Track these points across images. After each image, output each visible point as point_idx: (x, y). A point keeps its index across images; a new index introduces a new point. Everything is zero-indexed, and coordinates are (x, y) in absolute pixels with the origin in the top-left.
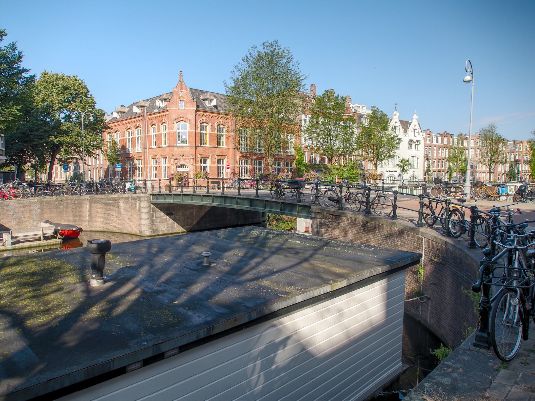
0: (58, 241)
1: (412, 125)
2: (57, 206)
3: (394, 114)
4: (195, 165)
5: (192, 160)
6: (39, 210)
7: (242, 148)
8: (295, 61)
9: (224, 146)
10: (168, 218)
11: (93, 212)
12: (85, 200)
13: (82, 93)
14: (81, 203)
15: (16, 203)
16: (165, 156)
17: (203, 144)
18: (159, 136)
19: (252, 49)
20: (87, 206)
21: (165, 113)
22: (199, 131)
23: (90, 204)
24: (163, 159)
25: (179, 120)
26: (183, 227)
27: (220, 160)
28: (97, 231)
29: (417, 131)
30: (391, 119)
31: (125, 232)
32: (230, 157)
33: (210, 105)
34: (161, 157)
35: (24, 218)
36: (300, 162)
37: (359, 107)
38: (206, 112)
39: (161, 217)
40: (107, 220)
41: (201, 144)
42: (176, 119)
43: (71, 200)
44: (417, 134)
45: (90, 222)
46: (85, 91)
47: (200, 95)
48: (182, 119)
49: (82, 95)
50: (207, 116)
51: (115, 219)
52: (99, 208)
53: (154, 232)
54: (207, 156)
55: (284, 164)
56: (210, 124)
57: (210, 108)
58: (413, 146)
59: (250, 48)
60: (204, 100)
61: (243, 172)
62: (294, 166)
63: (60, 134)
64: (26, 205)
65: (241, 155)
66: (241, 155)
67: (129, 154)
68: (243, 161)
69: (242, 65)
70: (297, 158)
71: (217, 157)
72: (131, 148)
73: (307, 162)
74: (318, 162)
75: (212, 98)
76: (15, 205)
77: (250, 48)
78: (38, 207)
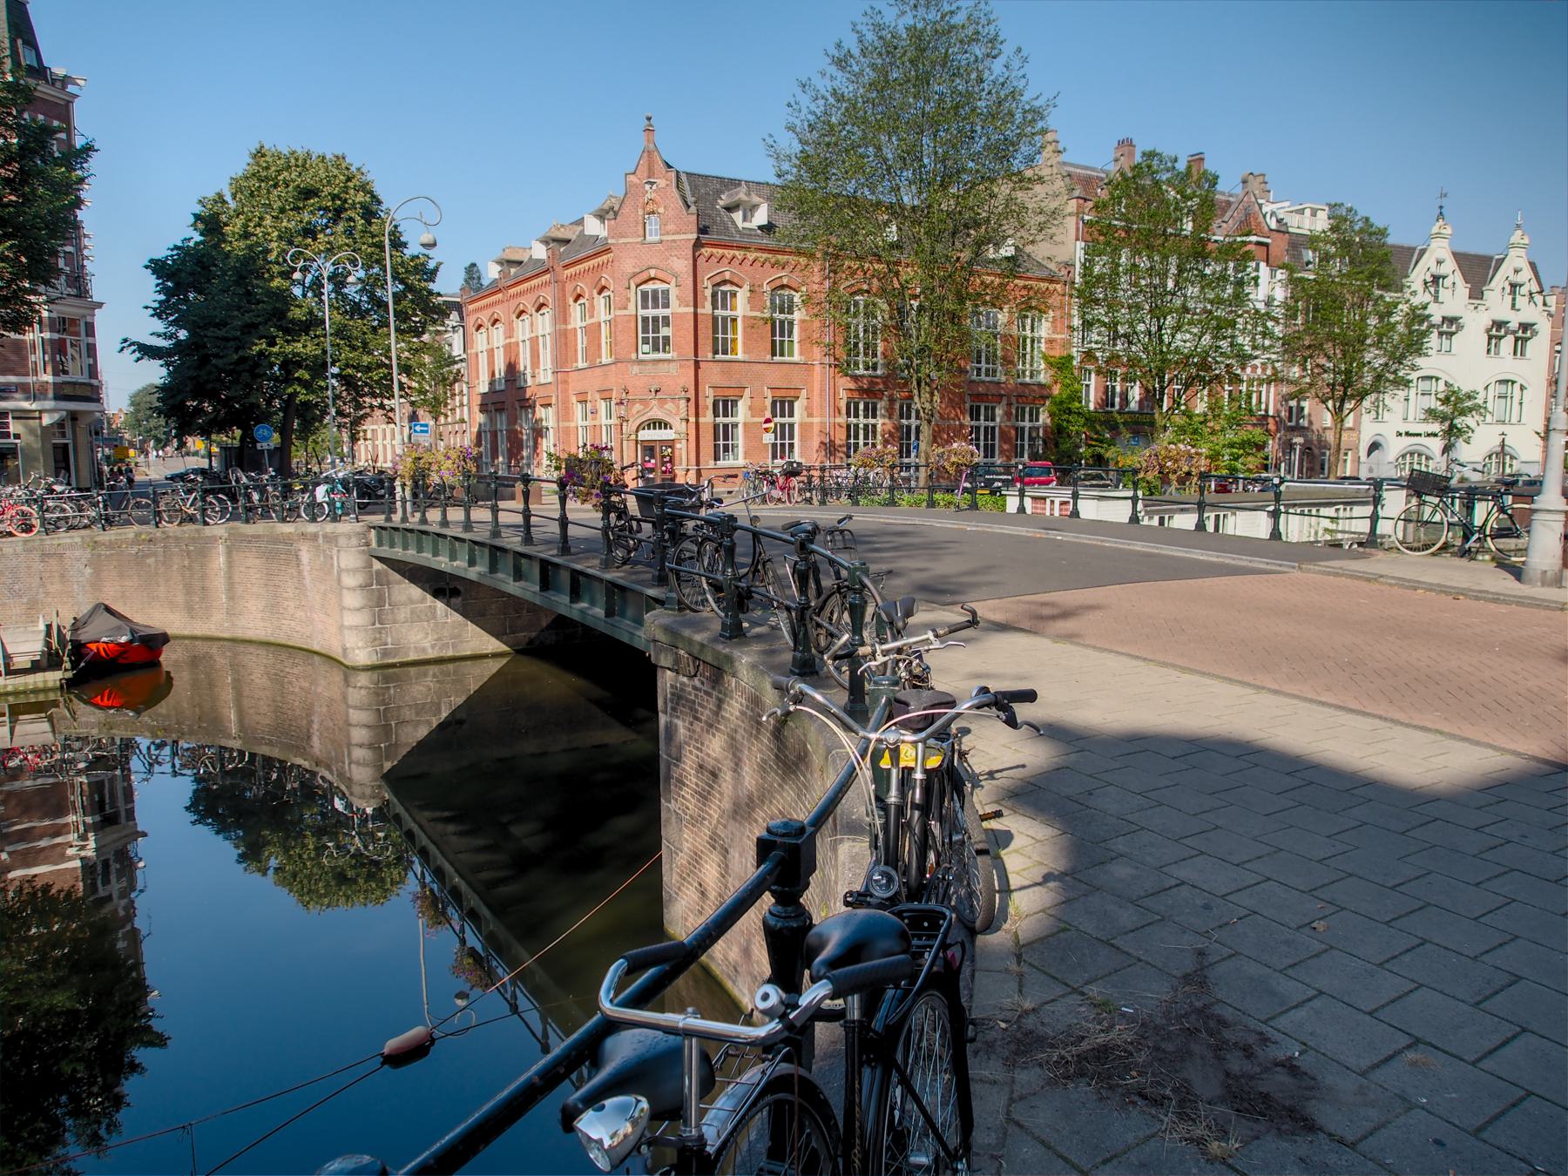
0: (53, 677)
1: (1505, 270)
2: (140, 559)
3: (1435, 230)
4: (692, 419)
5: (683, 403)
6: (88, 570)
7: (857, 364)
8: (1008, 49)
9: (796, 358)
10: (440, 605)
11: (237, 579)
12: (214, 539)
13: (353, 206)
14: (202, 551)
15: (19, 549)
16: (606, 395)
17: (725, 352)
18: (593, 331)
19: (865, 20)
20: (219, 560)
21: (605, 258)
22: (706, 309)
23: (229, 553)
24: (603, 403)
25: (644, 276)
26: (497, 636)
27: (782, 403)
28: (250, 642)
29: (1524, 290)
30: (1423, 252)
31: (316, 648)
32: (816, 392)
33: (747, 225)
34: (598, 396)
35: (47, 594)
36: (1064, 409)
37: (1301, 212)
38: (731, 247)
39: (411, 601)
40: (274, 608)
41: (716, 352)
42: (635, 275)
43: (177, 538)
44: (1522, 302)
45: (230, 613)
46: (360, 197)
47: (718, 193)
48: (653, 273)
49: (351, 213)
50: (725, 261)
51: (292, 604)
52: (251, 565)
53: (385, 653)
54: (737, 392)
55: (1008, 414)
56: (746, 287)
57: (748, 233)
58: (1507, 344)
59: (860, 19)
60: (729, 209)
61: (861, 442)
62: (1044, 418)
63: (287, 331)
64: (49, 555)
65: (852, 386)
66: (852, 386)
67: (523, 389)
68: (861, 406)
69: (832, 78)
70: (1056, 390)
71: (769, 394)
72: (528, 371)
73: (1092, 406)
74: (1133, 406)
75: (755, 199)
76: (16, 554)
77: (860, 19)
78: (84, 561)
